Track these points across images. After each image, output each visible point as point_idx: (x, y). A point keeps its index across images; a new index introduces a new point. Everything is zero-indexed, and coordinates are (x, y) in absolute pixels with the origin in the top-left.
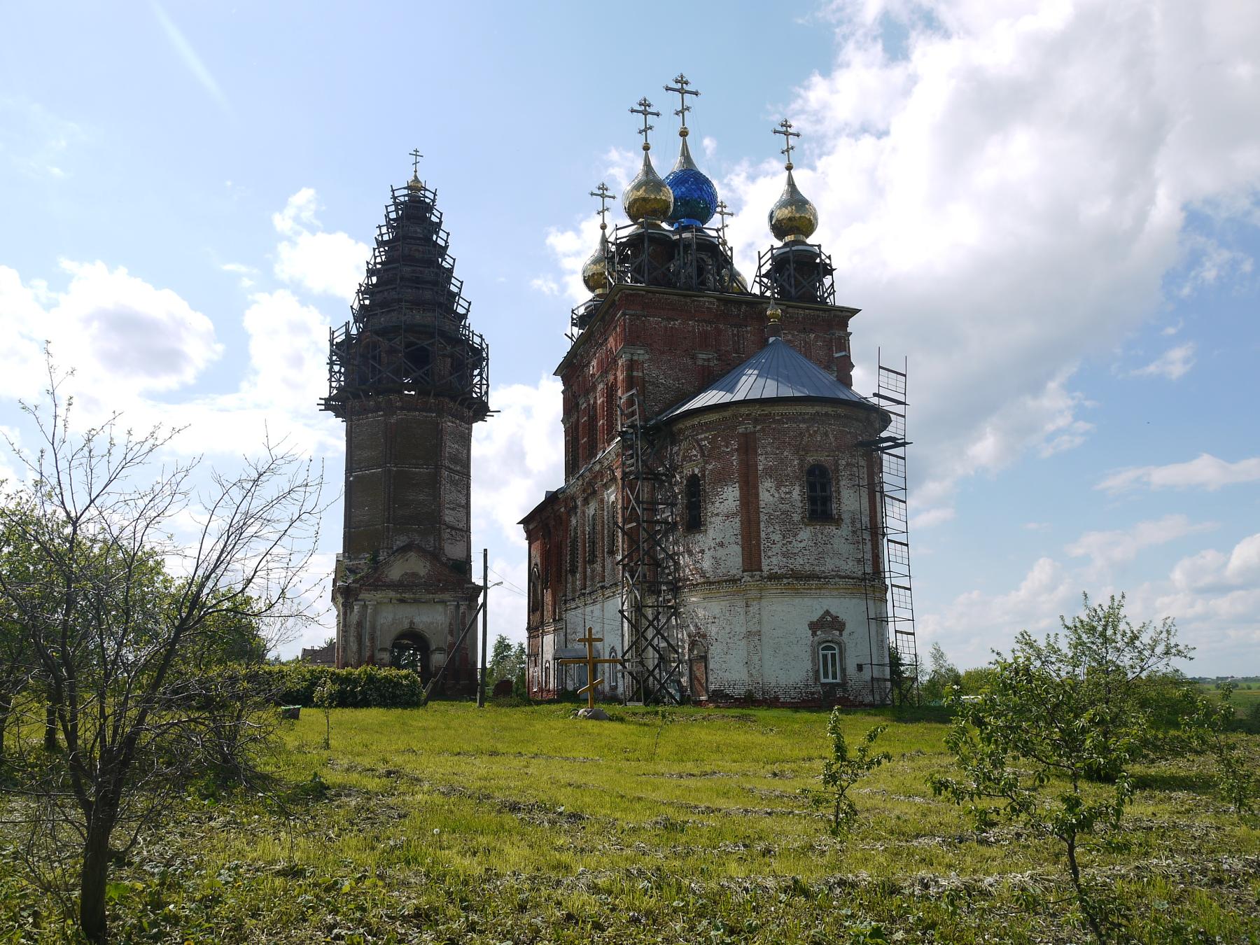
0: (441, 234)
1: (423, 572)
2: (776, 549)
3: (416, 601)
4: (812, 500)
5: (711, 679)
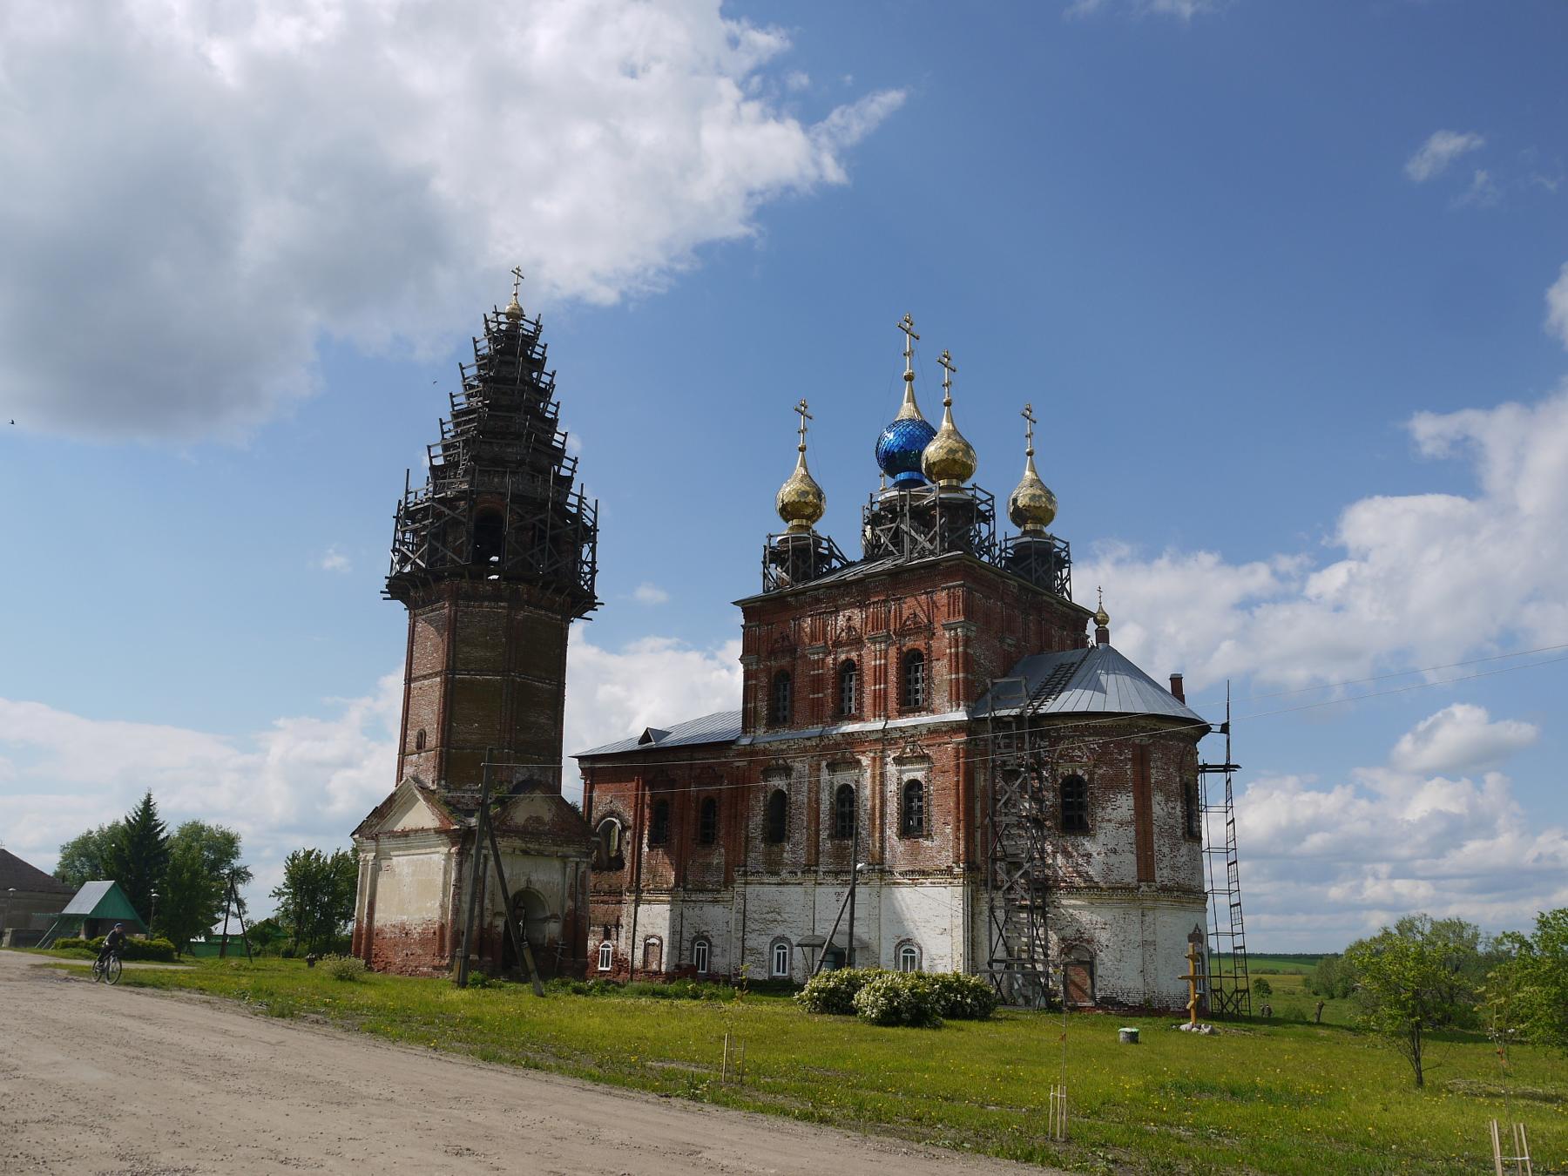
1: (547, 817)
2: (1166, 862)
3: (540, 854)
4: (1066, 806)
5: (1099, 984)
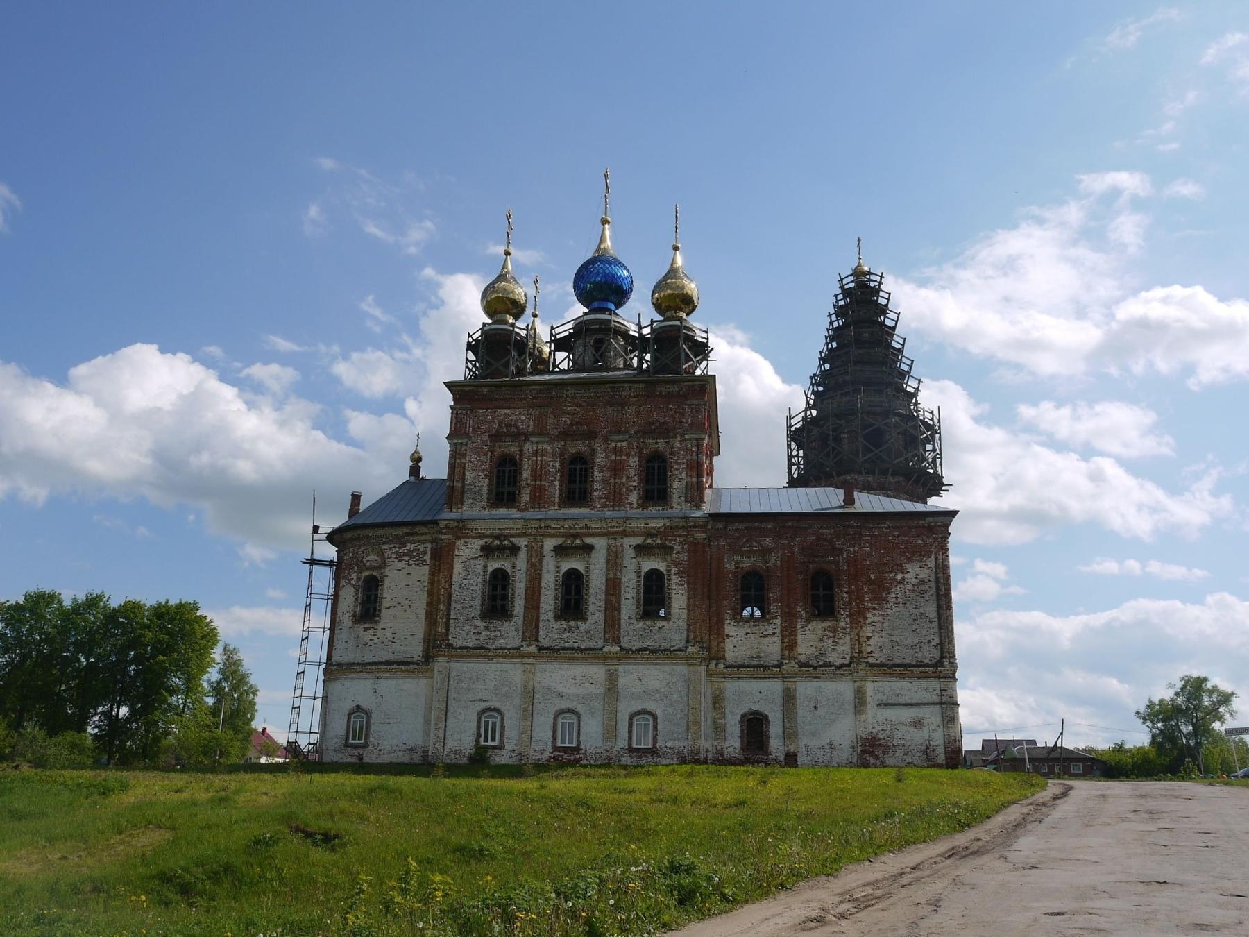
0: (891, 315)
